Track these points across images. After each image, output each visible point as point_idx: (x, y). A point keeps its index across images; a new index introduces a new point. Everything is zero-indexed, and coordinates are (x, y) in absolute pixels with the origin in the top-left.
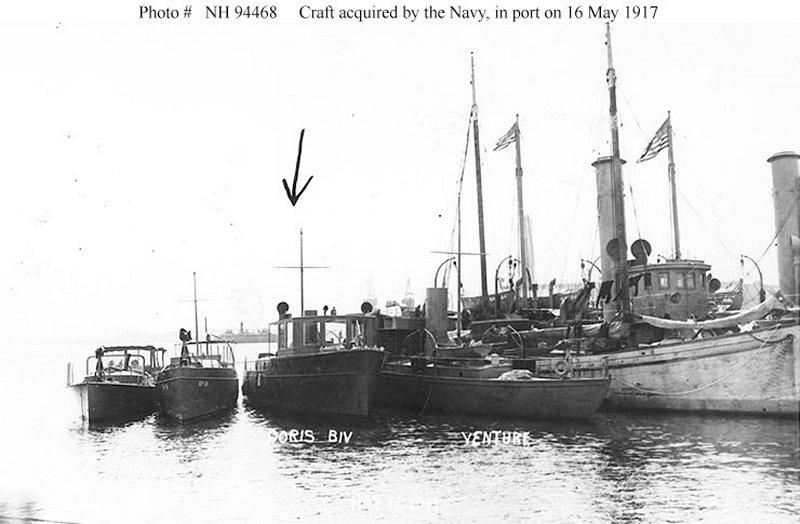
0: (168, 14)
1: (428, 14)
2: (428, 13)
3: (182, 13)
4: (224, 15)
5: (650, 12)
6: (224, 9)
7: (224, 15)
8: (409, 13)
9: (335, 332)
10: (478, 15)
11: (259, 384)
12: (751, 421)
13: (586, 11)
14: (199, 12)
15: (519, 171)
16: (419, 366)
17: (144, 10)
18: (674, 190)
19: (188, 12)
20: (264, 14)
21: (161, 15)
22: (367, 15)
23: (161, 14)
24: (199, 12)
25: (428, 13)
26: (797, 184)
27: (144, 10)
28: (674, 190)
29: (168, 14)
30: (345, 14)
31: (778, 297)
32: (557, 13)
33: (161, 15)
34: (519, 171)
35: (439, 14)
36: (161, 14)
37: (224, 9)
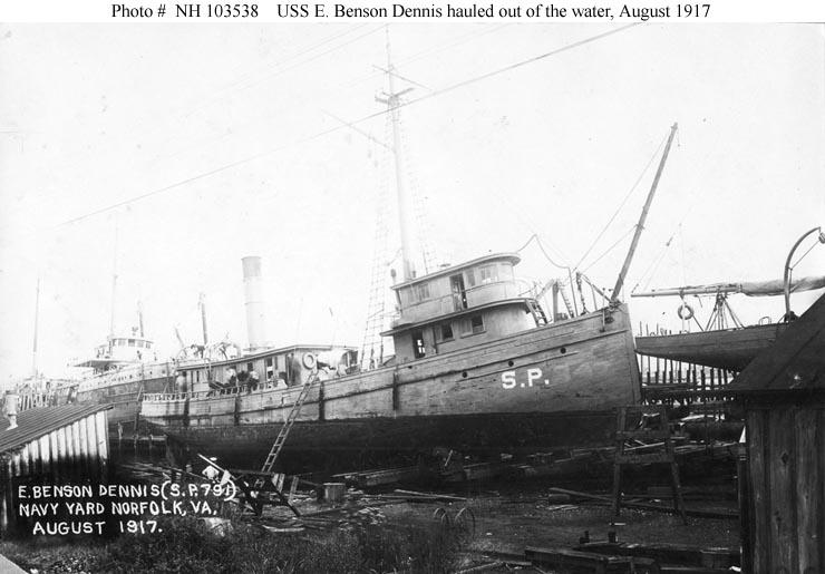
0: (141, 12)
1: (550, 14)
3: (156, 11)
4: (194, 13)
5: (702, 11)
6: (195, 8)
7: (194, 13)
8: (577, 13)
9: (117, 390)
12: (490, 411)
14: (171, 10)
15: (640, 227)
17: (117, 8)
18: (805, 236)
19: (162, 11)
21: (374, 13)
24: (171, 10)
26: (235, 570)
27: (117, 8)
28: (805, 236)
29: (141, 12)
30: (665, 12)
32: (383, 12)
33: (374, 13)
34: (640, 227)
35: (561, 14)
36: (374, 13)
37: (195, 8)
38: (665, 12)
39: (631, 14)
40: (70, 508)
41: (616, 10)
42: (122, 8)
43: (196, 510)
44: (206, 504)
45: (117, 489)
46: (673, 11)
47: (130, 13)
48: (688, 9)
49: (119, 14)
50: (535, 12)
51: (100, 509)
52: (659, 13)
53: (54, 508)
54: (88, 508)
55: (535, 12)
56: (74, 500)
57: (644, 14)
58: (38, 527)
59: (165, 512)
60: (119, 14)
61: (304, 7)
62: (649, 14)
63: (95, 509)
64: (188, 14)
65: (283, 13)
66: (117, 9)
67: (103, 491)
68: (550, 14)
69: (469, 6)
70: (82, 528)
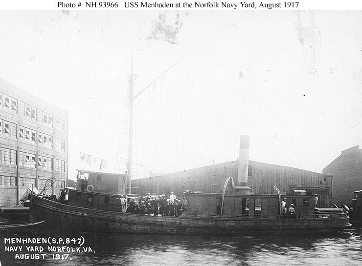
0: (70, 5)
1: (185, 6)
2: (185, 5)
3: (77, 5)
4: (94, 6)
5: (295, 5)
6: (94, 3)
7: (94, 6)
8: (171, 5)
10: (234, 6)
11: (235, 248)
13: (140, 4)
14: (84, 5)
16: (348, 211)
17: (60, 4)
19: (80, 5)
20: (109, 4)
22: (153, 5)
23: (68, 6)
24: (84, 5)
25: (185, 5)
27: (60, 4)
30: (279, 5)
31: (78, 196)
32: (172, 5)
35: (190, 6)
36: (68, 6)
37: (94, 3)
38: (279, 5)
39: (264, 6)
40: (28, 249)
41: (257, 4)
42: (62, 3)
43: (86, 251)
44: (89, 248)
45: (15, 240)
46: (283, 5)
47: (66, 6)
48: (289, 4)
49: (61, 6)
50: (178, 6)
51: (41, 249)
52: (276, 6)
53: (20, 249)
54: (36, 249)
55: (178, 6)
56: (30, 244)
57: (269, 6)
58: (17, 256)
59: (73, 251)
60: (61, 6)
61: (136, 3)
62: (272, 6)
63: (39, 249)
64: (91, 6)
65: (127, 5)
66: (60, 4)
67: (44, 241)
68: (185, 6)
69: (163, 3)
70: (35, 257)
